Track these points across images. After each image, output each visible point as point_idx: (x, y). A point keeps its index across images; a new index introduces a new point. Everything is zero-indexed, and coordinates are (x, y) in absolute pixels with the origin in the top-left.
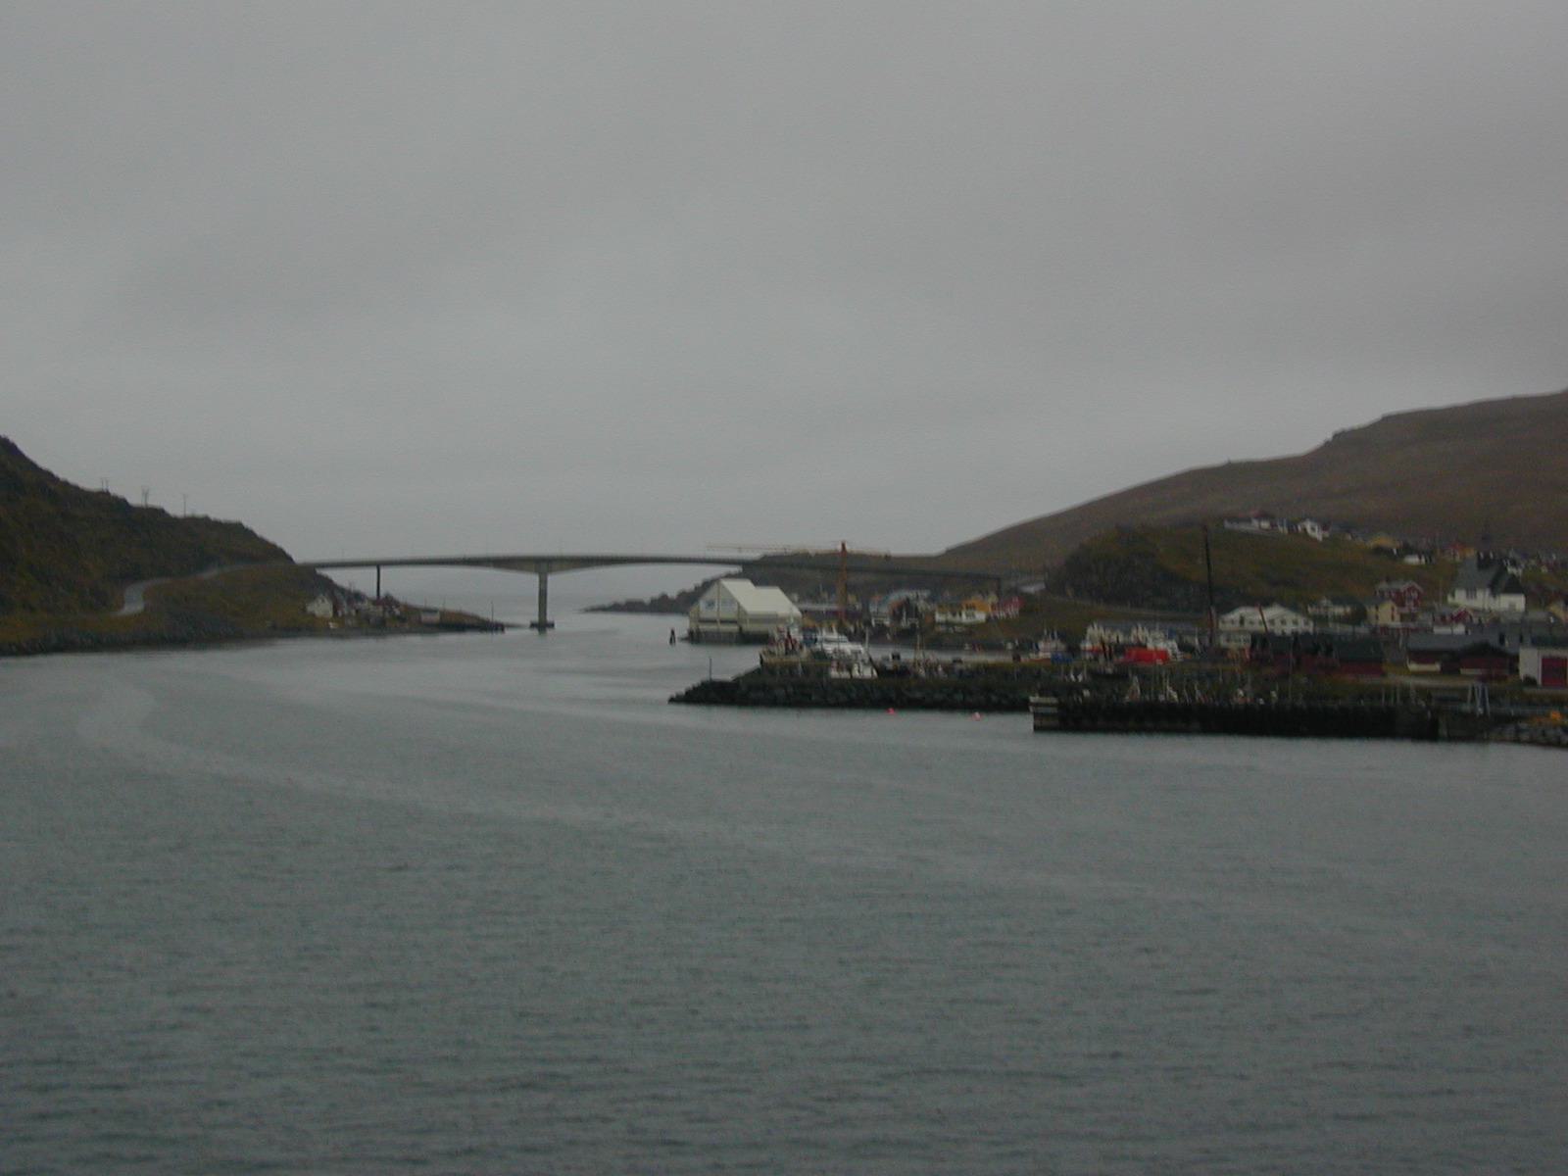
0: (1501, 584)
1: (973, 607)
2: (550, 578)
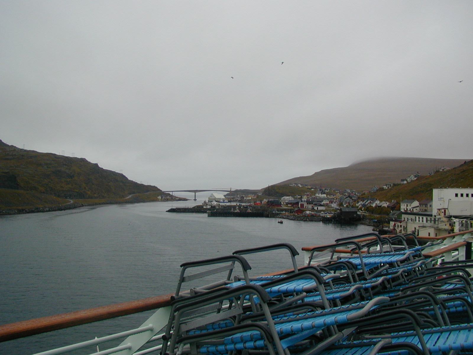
0: (323, 193)
1: (249, 197)
2: (196, 193)
